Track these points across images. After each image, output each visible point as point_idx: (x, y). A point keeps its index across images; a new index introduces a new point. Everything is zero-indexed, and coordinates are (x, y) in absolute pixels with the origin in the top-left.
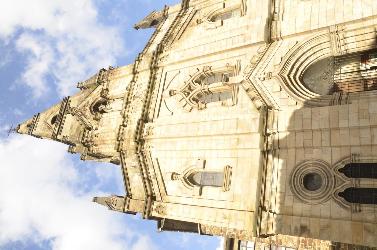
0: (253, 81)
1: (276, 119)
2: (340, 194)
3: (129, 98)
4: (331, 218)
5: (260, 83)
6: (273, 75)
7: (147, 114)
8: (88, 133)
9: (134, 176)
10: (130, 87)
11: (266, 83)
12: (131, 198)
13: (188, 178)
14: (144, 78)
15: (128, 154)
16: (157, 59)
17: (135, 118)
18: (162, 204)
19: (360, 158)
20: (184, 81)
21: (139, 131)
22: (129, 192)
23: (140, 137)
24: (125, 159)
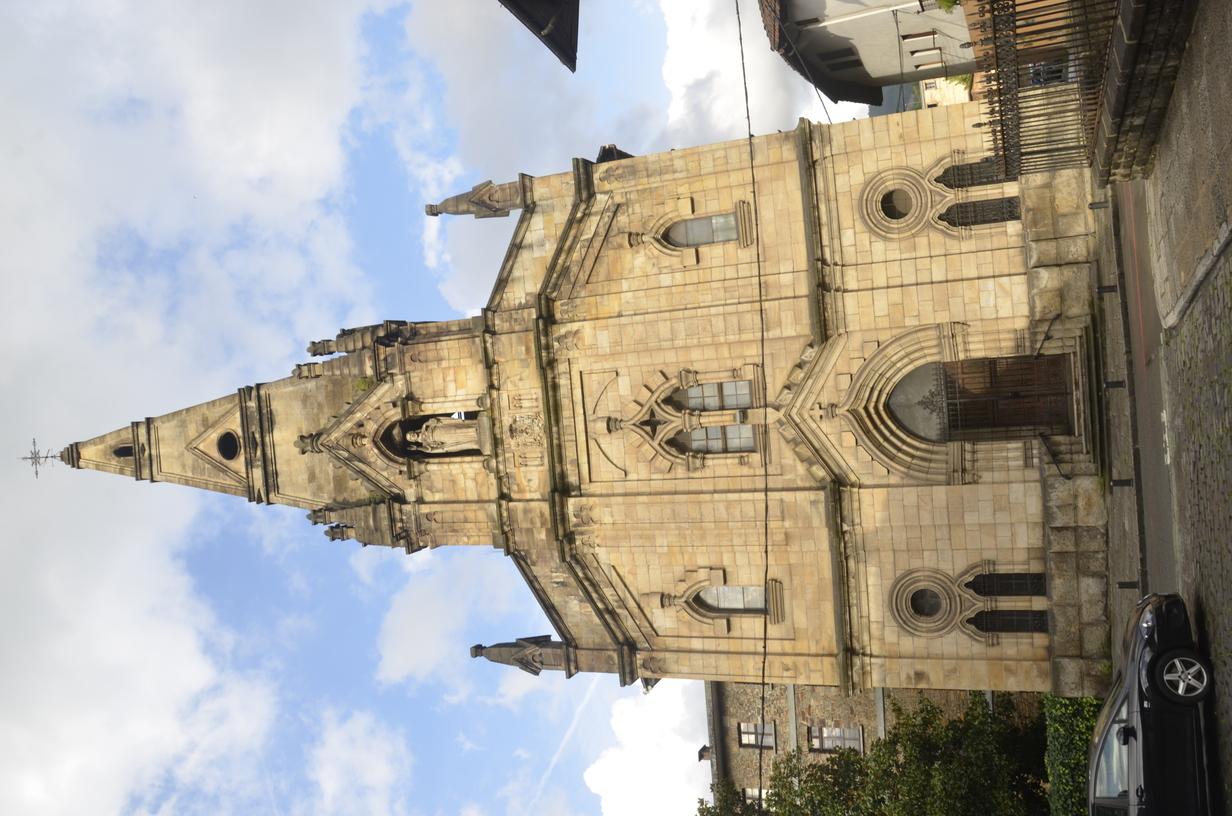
0: (798, 420)
1: (856, 505)
2: (969, 621)
3: (497, 431)
4: (958, 658)
5: (814, 426)
6: (838, 411)
7: (563, 475)
8: (401, 511)
9: (566, 602)
10: (491, 404)
11: (826, 426)
12: (576, 647)
13: (694, 600)
14: (521, 379)
15: (534, 557)
16: (550, 340)
17: (529, 480)
18: (654, 654)
19: (996, 567)
20: (633, 398)
21: (559, 517)
22: (568, 636)
23: (565, 530)
24: (532, 567)
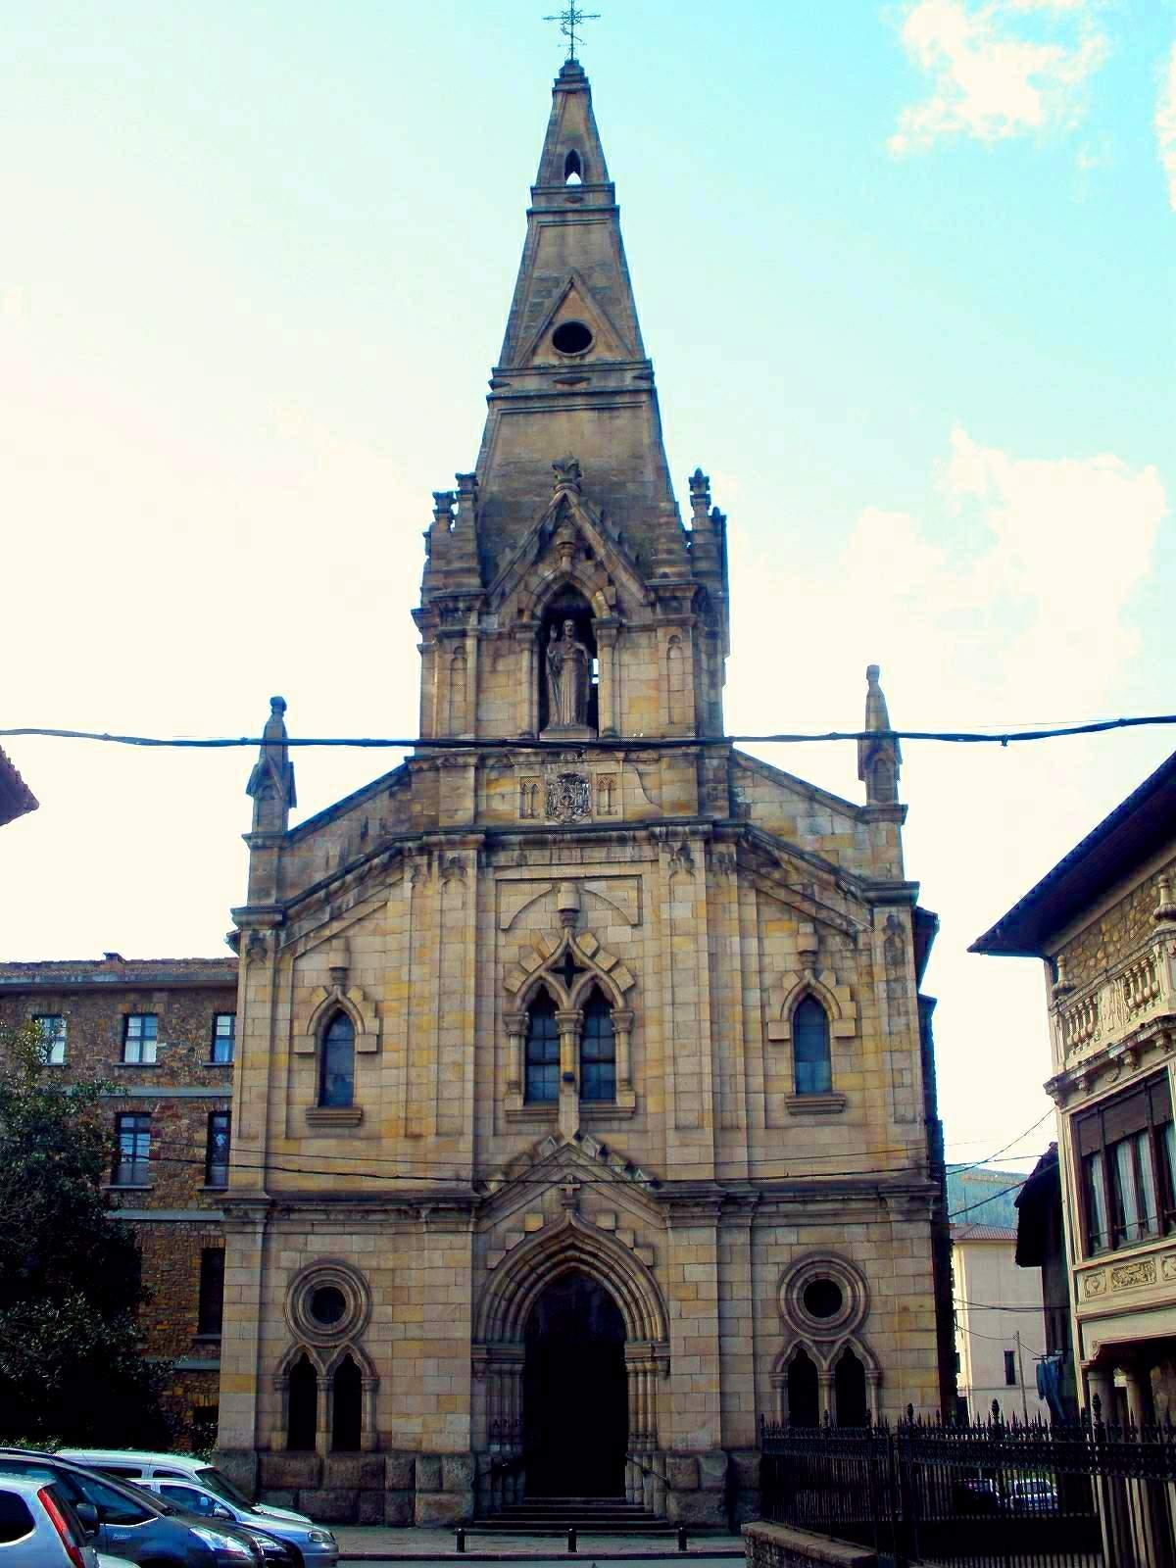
2: (305, 1357)
